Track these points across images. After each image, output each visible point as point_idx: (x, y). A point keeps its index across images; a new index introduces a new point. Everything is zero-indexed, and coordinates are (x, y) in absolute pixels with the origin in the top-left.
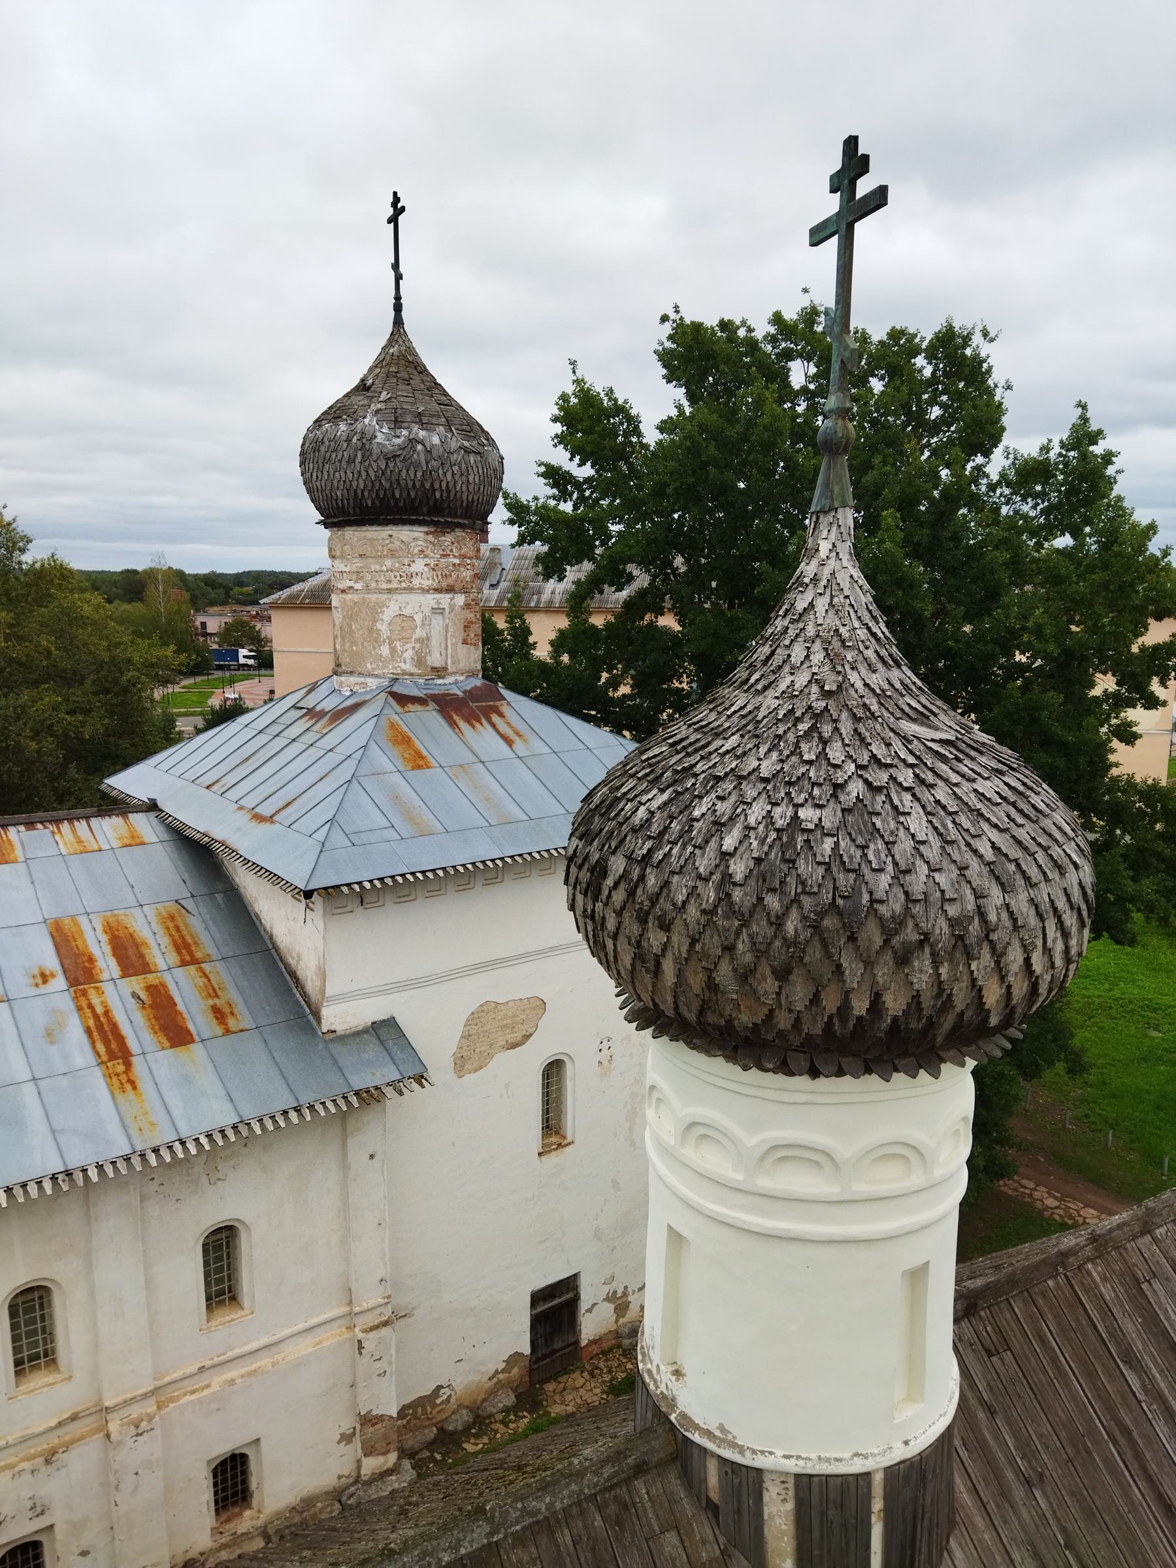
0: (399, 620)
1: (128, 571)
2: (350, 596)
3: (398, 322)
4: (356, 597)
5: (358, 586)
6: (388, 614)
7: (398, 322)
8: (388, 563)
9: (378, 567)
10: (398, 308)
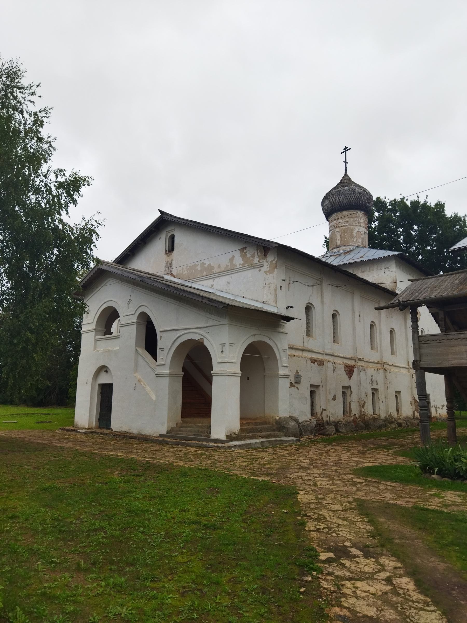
0: (358, 233)
1: (365, 191)
2: (344, 227)
3: (346, 173)
4: (346, 227)
5: (347, 224)
6: (356, 231)
7: (346, 173)
8: (356, 219)
9: (353, 220)
10: (346, 170)
